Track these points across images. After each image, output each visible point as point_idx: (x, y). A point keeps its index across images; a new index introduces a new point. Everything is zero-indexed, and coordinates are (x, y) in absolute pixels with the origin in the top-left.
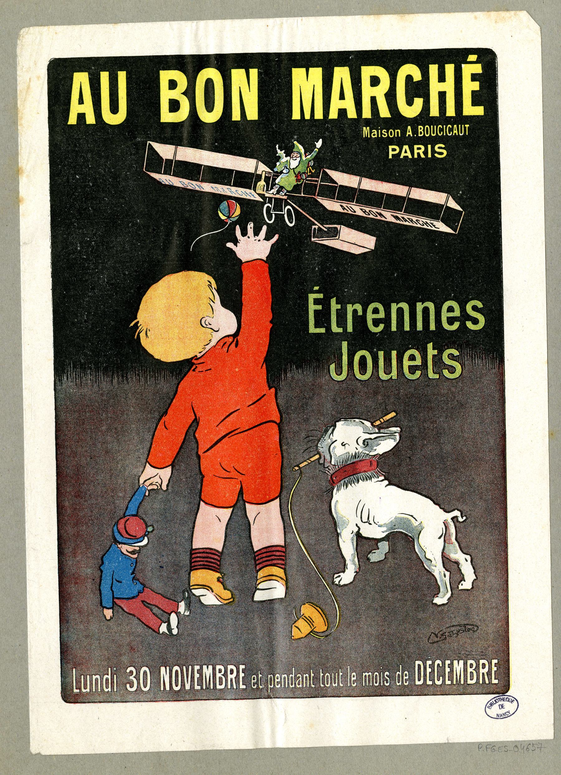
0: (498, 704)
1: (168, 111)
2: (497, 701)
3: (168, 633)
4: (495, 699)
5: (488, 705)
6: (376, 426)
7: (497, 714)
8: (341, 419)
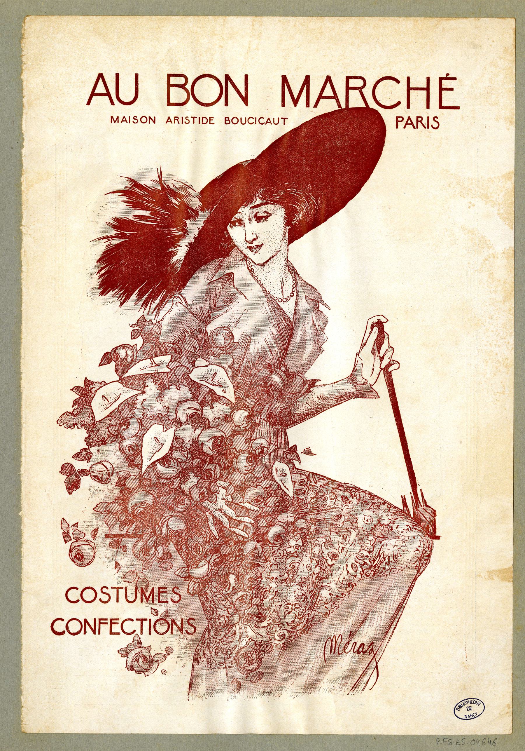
0: (466, 706)
4: (463, 702)
5: (457, 707)
7: (465, 716)
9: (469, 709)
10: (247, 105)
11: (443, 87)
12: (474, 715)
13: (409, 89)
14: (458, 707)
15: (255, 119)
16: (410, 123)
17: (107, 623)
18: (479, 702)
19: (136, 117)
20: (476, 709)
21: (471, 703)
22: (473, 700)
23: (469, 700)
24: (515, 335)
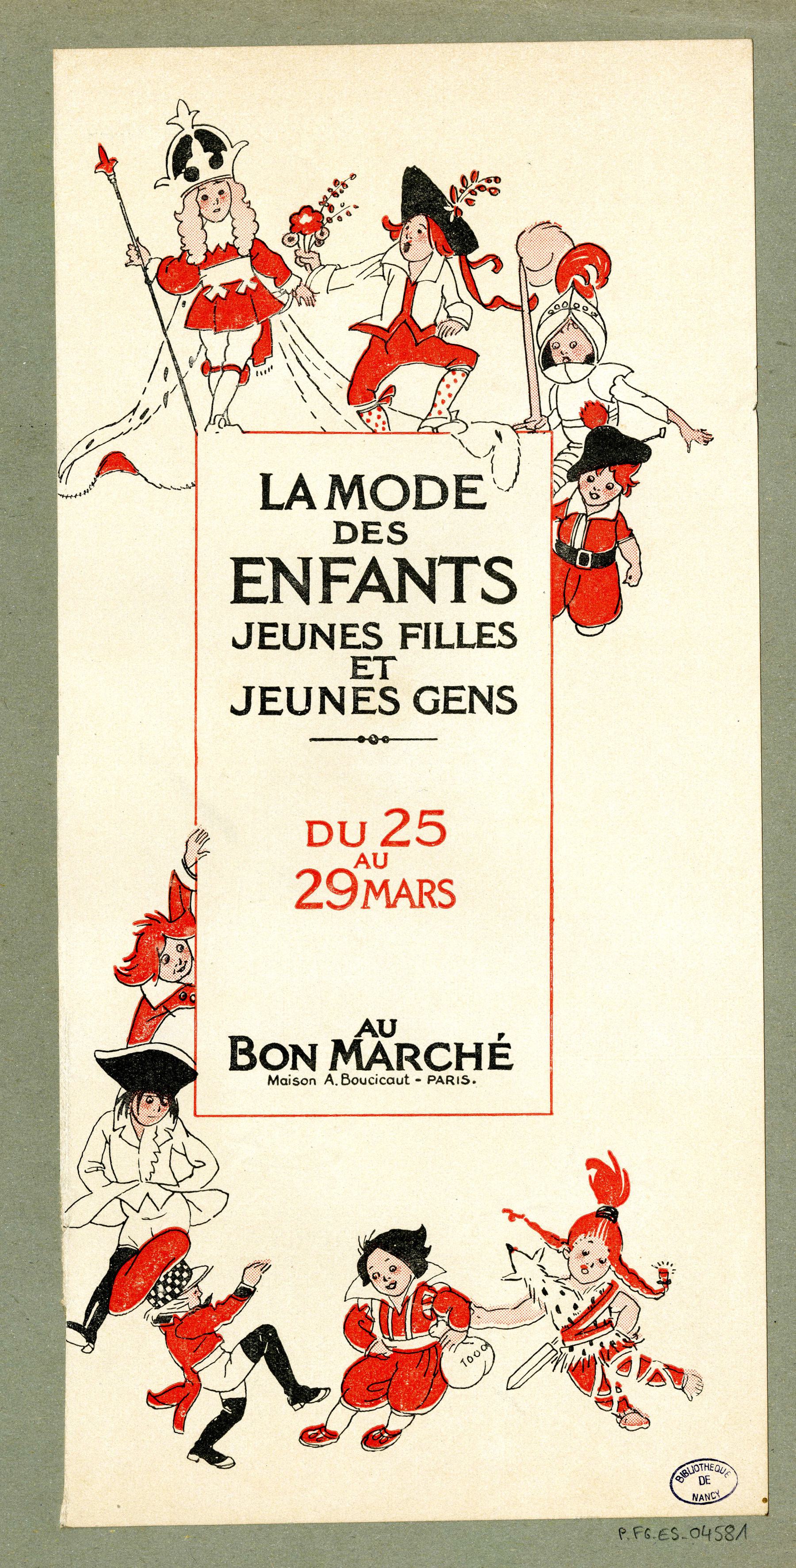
0: (697, 1474)
1: (587, 401)
2: (697, 1468)
3: (555, 550)
4: (693, 1464)
5: (678, 1474)
6: (563, 1243)
7: (694, 1495)
8: (187, 1374)
12: (714, 1495)
14: (681, 1474)
16: (369, 583)
17: (386, 855)
19: (377, 626)
21: (710, 1468)
22: (716, 1463)
23: (707, 1462)
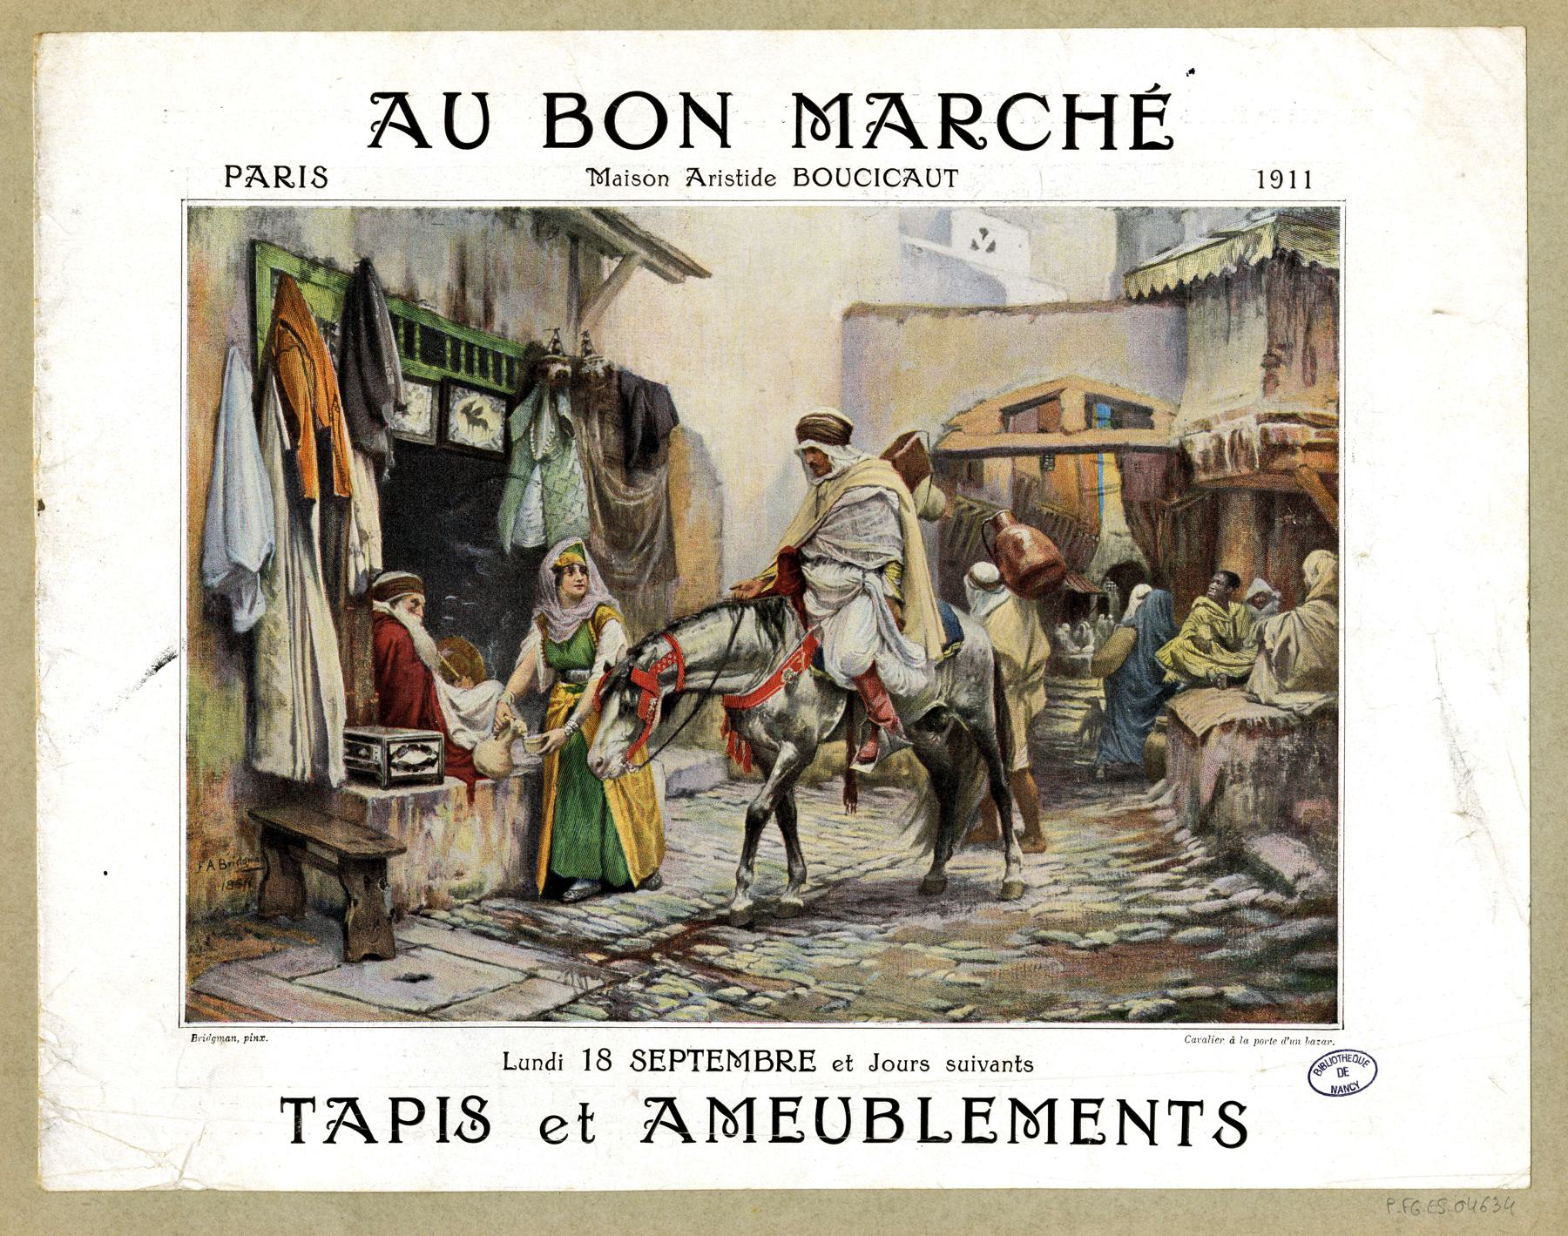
0: (1335, 1067)
5: (1316, 1067)
9: (1344, 1072)
10: (695, 271)
11: (303, 1105)
13: (1072, 115)
15: (874, 172)
18: (1367, 1058)
20: (1358, 1074)
21: (1347, 1059)
24: (1533, 664)
